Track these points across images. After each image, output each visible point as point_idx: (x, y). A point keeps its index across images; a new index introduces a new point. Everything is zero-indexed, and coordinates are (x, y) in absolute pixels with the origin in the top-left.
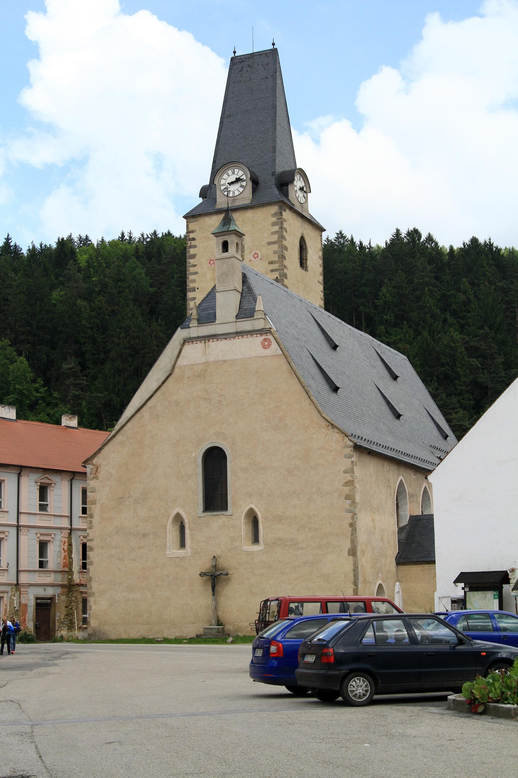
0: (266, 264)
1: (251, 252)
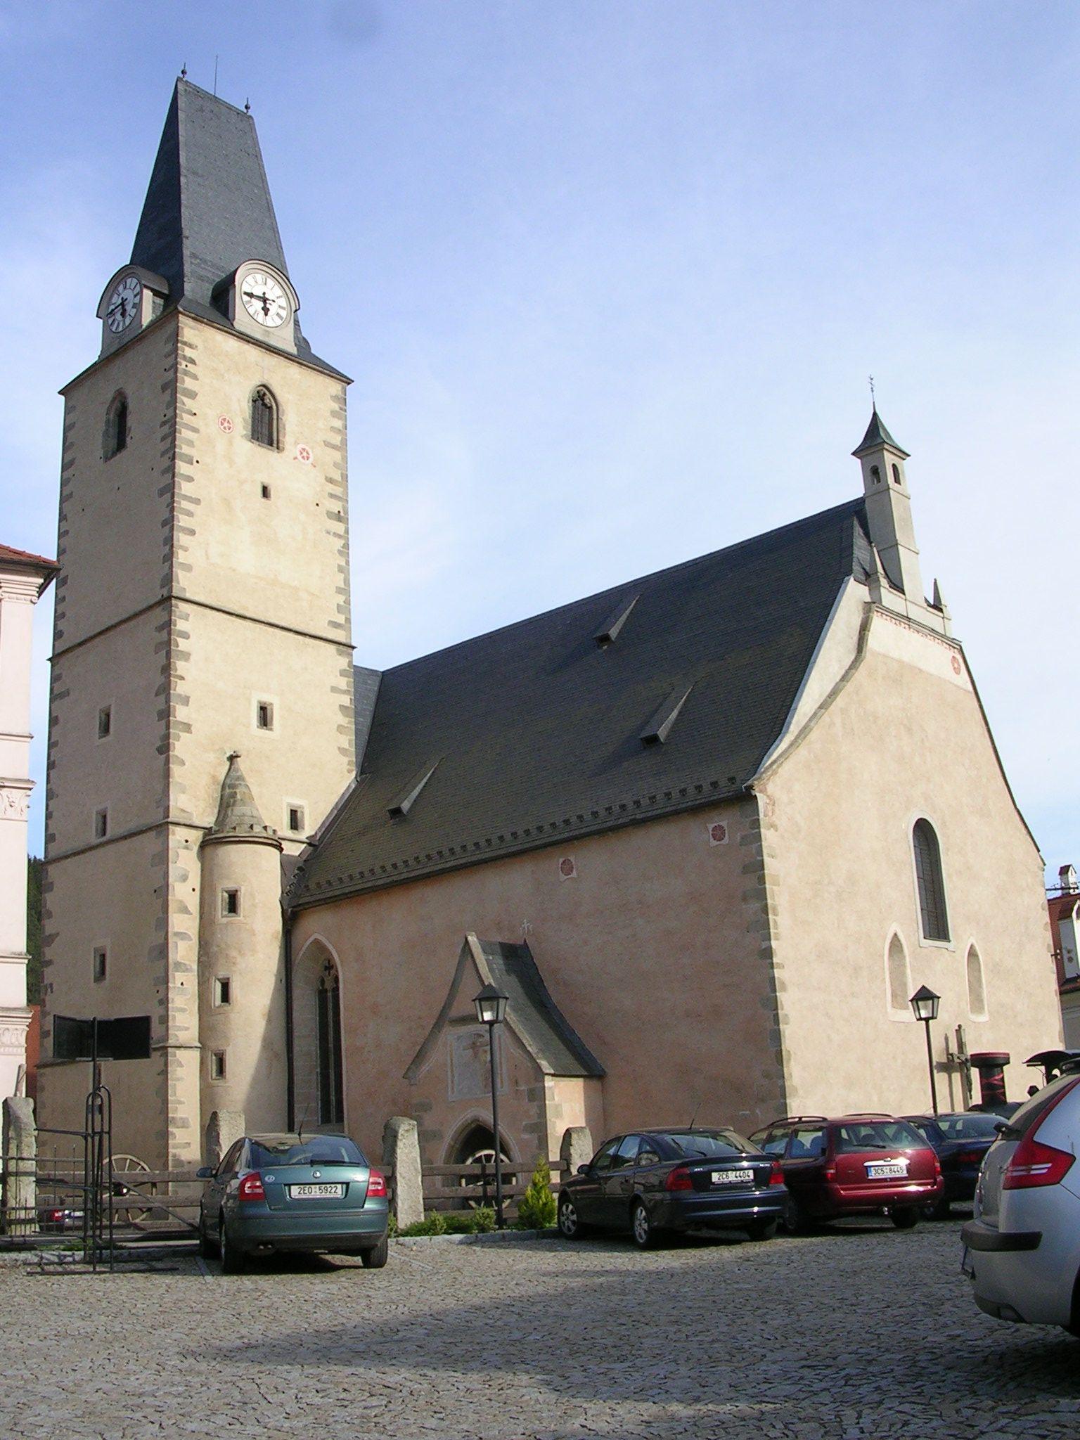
1: (296, 443)
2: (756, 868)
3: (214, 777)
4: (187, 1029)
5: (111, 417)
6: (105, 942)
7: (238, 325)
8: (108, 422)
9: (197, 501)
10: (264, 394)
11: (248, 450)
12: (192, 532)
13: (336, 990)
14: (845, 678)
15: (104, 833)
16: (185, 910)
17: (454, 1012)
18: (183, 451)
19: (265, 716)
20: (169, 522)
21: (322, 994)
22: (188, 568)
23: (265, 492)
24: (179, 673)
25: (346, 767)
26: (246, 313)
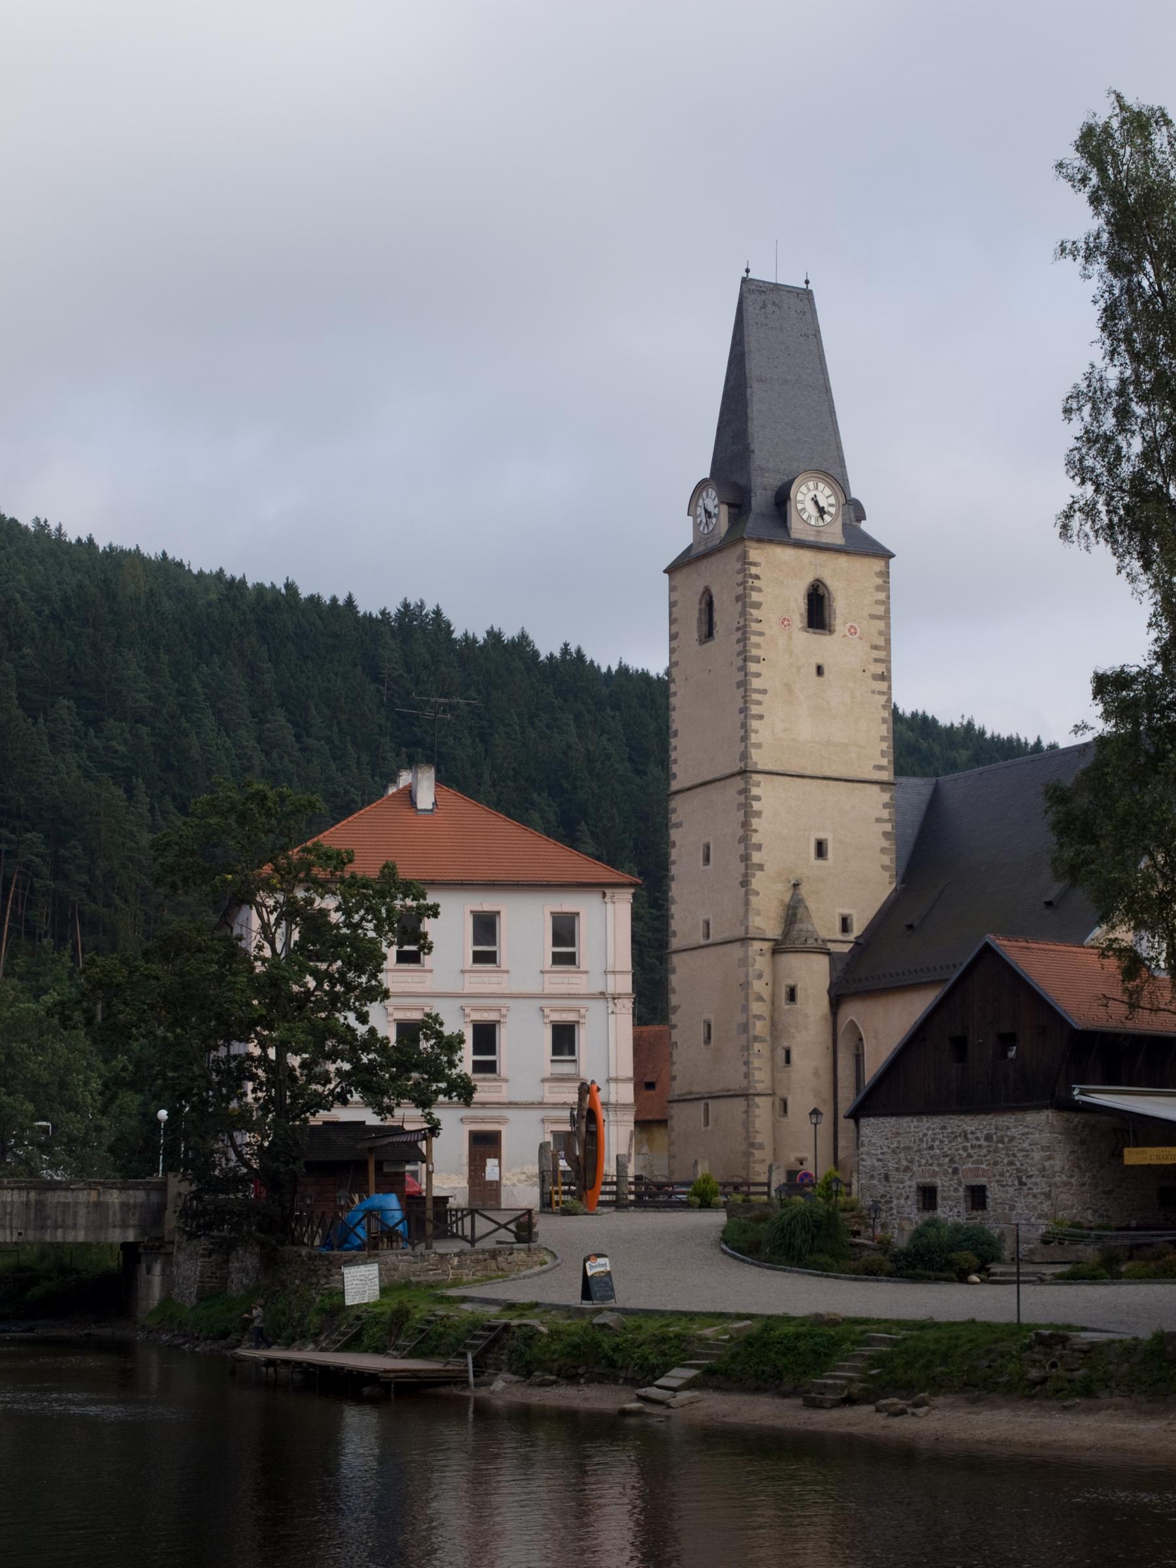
0: (868, 649)
1: (845, 623)
3: (782, 901)
4: (763, 1082)
6: (711, 1016)
8: (700, 610)
9: (764, 692)
10: (818, 586)
11: (804, 639)
12: (761, 717)
15: (708, 936)
16: (760, 999)
19: (821, 849)
22: (759, 746)
23: (820, 670)
25: (888, 880)
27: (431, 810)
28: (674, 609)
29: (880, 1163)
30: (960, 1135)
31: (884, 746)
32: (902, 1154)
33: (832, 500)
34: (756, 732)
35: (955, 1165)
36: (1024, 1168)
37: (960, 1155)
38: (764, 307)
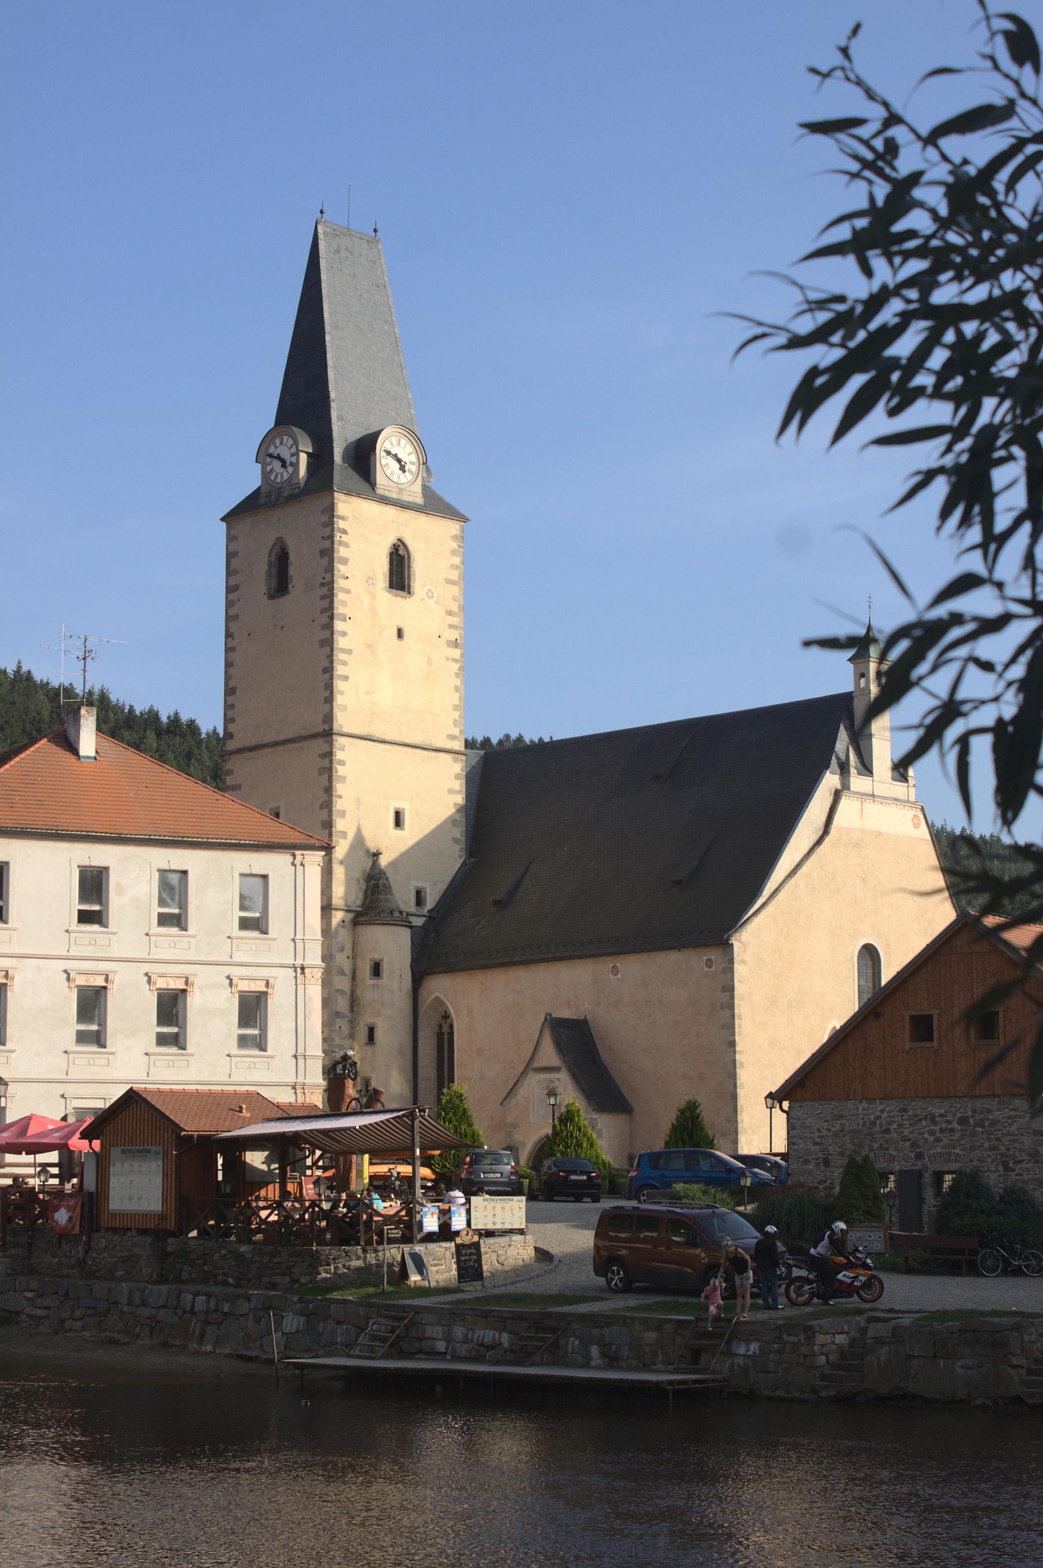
1: (423, 586)
2: (730, 989)
5: (273, 559)
7: (380, 491)
10: (399, 546)
13: (451, 1034)
14: (811, 850)
16: (342, 973)
17: (536, 1065)
18: (339, 611)
19: (398, 820)
20: (329, 670)
21: (440, 1036)
23: (400, 634)
24: (338, 793)
26: (385, 469)
27: (95, 758)
28: (233, 561)
29: (817, 1147)
30: (926, 1118)
31: (456, 715)
32: (847, 1138)
33: (413, 458)
34: (342, 693)
35: (918, 1150)
36: (1011, 1152)
37: (924, 1139)
38: (338, 251)
